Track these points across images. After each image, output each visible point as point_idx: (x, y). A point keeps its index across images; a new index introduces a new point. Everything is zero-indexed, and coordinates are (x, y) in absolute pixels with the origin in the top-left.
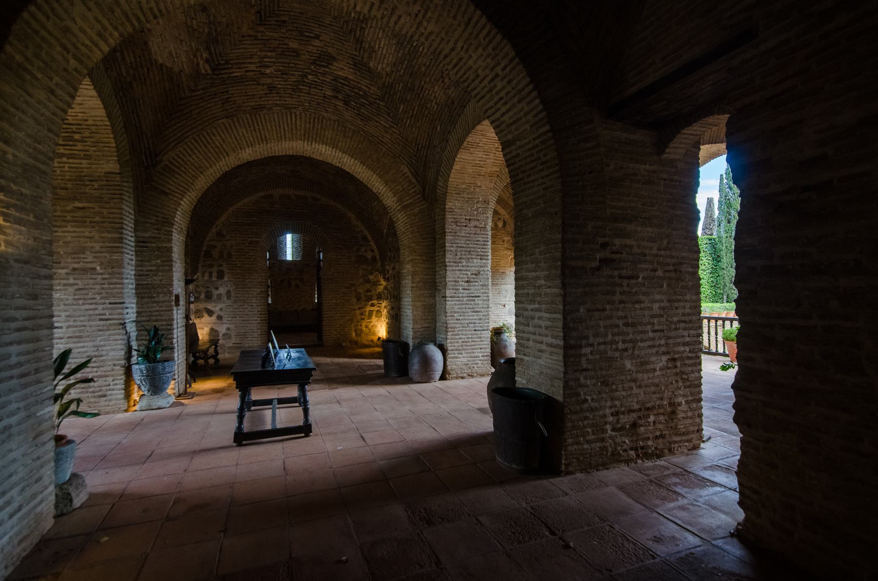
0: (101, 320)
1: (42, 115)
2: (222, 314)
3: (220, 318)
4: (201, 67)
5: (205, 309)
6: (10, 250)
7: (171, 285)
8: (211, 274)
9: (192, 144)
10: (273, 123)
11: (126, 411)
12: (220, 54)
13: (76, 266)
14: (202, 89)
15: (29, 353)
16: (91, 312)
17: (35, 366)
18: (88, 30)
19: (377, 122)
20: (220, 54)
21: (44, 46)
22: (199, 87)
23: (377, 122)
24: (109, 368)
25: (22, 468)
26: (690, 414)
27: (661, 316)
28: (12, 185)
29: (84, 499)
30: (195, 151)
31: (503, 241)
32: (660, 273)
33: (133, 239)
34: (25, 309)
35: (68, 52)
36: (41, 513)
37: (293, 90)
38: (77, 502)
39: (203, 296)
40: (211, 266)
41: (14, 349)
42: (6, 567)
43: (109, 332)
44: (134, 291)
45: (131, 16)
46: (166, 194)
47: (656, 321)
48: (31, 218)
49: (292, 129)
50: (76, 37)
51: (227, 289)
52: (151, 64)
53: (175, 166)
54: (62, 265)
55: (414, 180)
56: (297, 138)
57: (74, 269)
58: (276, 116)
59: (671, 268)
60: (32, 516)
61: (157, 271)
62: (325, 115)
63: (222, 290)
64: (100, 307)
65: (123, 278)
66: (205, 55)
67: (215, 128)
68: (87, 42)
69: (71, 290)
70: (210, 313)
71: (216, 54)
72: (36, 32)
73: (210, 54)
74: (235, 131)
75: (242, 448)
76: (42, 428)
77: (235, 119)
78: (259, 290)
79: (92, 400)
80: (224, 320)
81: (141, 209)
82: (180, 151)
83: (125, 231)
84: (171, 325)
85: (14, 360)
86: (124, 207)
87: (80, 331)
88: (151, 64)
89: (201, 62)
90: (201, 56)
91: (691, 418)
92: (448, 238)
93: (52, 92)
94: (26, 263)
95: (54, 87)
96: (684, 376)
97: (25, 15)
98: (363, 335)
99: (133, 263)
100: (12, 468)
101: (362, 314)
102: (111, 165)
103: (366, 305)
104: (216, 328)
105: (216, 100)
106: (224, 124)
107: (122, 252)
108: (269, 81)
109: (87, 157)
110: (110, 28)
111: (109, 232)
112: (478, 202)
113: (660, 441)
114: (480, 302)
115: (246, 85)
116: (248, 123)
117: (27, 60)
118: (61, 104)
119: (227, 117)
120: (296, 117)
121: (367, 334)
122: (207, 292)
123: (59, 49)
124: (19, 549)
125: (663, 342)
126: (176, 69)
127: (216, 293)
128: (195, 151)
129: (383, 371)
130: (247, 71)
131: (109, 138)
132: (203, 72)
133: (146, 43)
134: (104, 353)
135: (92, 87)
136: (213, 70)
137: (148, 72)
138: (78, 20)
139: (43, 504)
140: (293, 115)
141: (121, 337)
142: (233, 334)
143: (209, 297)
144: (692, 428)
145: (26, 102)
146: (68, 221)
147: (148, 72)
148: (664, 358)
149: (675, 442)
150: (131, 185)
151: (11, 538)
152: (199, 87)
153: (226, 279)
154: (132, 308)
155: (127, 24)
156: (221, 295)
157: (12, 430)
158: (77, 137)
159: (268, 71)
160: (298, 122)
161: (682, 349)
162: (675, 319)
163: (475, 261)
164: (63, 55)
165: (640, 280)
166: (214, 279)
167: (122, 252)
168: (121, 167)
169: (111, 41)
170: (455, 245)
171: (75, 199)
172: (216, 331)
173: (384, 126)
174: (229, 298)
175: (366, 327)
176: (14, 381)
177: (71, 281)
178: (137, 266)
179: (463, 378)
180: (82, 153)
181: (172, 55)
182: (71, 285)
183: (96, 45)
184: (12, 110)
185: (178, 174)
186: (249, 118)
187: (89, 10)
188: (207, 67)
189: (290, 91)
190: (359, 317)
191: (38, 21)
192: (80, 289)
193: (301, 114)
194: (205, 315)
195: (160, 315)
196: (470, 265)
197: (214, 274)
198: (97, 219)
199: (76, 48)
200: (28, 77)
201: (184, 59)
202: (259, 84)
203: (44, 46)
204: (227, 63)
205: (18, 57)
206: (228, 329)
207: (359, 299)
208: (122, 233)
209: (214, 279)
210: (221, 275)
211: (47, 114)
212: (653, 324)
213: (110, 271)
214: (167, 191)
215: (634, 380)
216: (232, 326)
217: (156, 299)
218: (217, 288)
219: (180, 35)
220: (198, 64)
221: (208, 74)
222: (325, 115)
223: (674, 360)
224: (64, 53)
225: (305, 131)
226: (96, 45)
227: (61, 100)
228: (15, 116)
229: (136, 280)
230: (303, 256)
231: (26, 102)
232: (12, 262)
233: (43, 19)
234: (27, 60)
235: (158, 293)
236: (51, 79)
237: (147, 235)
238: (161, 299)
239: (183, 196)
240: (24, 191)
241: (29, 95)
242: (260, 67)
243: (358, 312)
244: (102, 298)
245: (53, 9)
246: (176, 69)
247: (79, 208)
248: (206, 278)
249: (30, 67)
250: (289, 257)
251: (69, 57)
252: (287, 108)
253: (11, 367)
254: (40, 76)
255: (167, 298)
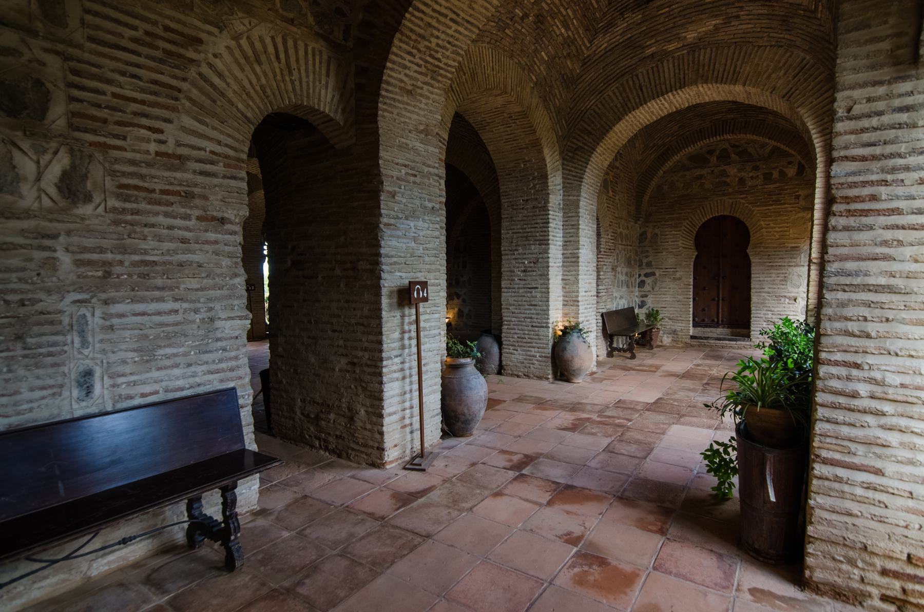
3: (464, 301)
26: (368, 426)
27: (339, 316)
31: (798, 197)
32: (338, 272)
47: (334, 320)
59: (349, 265)
91: (369, 430)
92: (505, 224)
96: (364, 384)
112: (534, 178)
113: (340, 441)
114: (539, 295)
118: (659, 90)
125: (341, 343)
144: (371, 443)
148: (344, 361)
149: (353, 449)
161: (360, 354)
162: (353, 321)
163: (533, 247)
165: (320, 279)
170: (510, 232)
179: (518, 376)
196: (527, 252)
212: (332, 324)
215: (318, 375)
223: (353, 364)
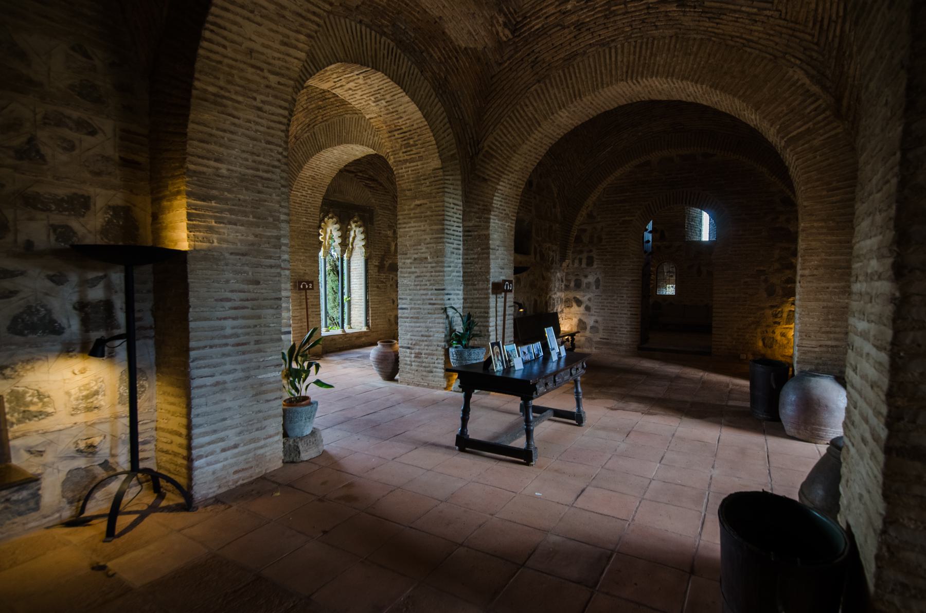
0: (430, 304)
1: (256, 131)
2: (590, 304)
3: (588, 309)
4: (501, 34)
5: (575, 298)
6: (225, 245)
7: (488, 273)
8: (580, 263)
9: (507, 122)
10: (588, 70)
11: (445, 389)
12: (515, 11)
13: (416, 256)
14: (509, 59)
15: (244, 327)
16: (424, 297)
17: (256, 338)
18: (270, 43)
19: (735, 11)
20: (515, 11)
21: (234, 72)
22: (505, 58)
23: (735, 11)
24: (434, 348)
25: (238, 416)
28: (226, 193)
29: (313, 456)
30: (510, 129)
33: (461, 229)
34: (240, 291)
35: (262, 70)
36: (263, 456)
37: (606, 17)
38: (305, 456)
39: (572, 284)
40: (581, 252)
41: (229, 323)
42: (220, 487)
43: (435, 316)
44: (461, 279)
45: (304, 13)
46: (485, 180)
48: (251, 219)
49: (611, 71)
50: (263, 54)
51: (596, 277)
52: (457, 52)
53: (493, 150)
54: (408, 256)
55: (815, 89)
56: (617, 81)
57: (415, 259)
58: (591, 60)
60: (251, 455)
61: (478, 259)
62: (656, 33)
63: (591, 279)
64: (430, 292)
65: (444, 267)
66: (501, 20)
67: (528, 98)
68: (277, 55)
69: (413, 276)
70: (579, 303)
71: (510, 13)
72: (220, 62)
73: (505, 15)
74: (547, 95)
75: (462, 454)
76: (264, 388)
77: (547, 81)
78: (630, 279)
79: (424, 373)
80: (592, 312)
81: (468, 199)
82: (498, 134)
83: (446, 222)
84: (488, 313)
85: (228, 331)
86: (446, 199)
87: (418, 313)
88: (457, 52)
89: (500, 29)
90: (498, 22)
93: (260, 109)
94: (243, 255)
95: (261, 105)
97: (201, 52)
98: (776, 347)
99: (461, 252)
100: (227, 414)
101: (775, 316)
102: (436, 163)
103: (783, 303)
104: (585, 320)
105: (525, 65)
106: (536, 90)
107: (443, 242)
108: (574, 18)
109: (421, 158)
110: (294, 34)
111: (436, 224)
115: (550, 36)
116: (561, 81)
117: (221, 88)
119: (539, 81)
120: (616, 52)
121: (784, 346)
122: (576, 280)
123: (251, 70)
124: (236, 477)
126: (480, 48)
127: (585, 281)
128: (510, 129)
129: (748, 405)
130: (547, 18)
131: (429, 136)
132: (505, 39)
133: (444, 33)
134: (431, 334)
135: (404, 94)
136: (513, 32)
137: (458, 61)
138: (254, 37)
139: (267, 449)
140: (613, 51)
141: (442, 321)
142: (601, 328)
143: (578, 286)
145: (234, 124)
146: (411, 218)
147: (458, 61)
150: (460, 177)
151: (224, 466)
152: (505, 58)
153: (595, 266)
154: (458, 294)
155: (307, 23)
156: (590, 283)
157: (226, 385)
158: (411, 142)
159: (569, 7)
160: (619, 58)
164: (258, 75)
166: (584, 265)
167: (443, 242)
168: (443, 162)
169: (301, 45)
171: (415, 198)
172: (584, 323)
173: (749, 14)
174: (597, 287)
175: (783, 335)
176: (229, 348)
177: (413, 270)
178: (464, 254)
180: (417, 156)
181: (471, 34)
182: (413, 273)
183: (289, 55)
184: (221, 133)
185: (497, 158)
186: (562, 74)
187: (260, 25)
188: (507, 32)
189: (601, 21)
190: (771, 320)
191: (216, 53)
192: (418, 277)
193: (623, 45)
194: (574, 304)
195: (479, 303)
197: (584, 261)
198: (429, 213)
199: (269, 64)
200: (229, 103)
201: (483, 33)
202: (564, 28)
203: (234, 72)
204: (525, 18)
205: (211, 89)
206: (596, 322)
207: (771, 292)
208: (443, 225)
209: (584, 265)
210: (590, 262)
211: (262, 129)
213: (436, 259)
214: (487, 177)
216: (599, 319)
217: (477, 287)
218: (586, 276)
219: (469, 10)
220: (498, 33)
221: (509, 40)
222: (656, 33)
224: (258, 72)
225: (628, 67)
226: (289, 55)
227: (273, 114)
228: (223, 138)
229: (463, 268)
230: (718, 236)
231: (234, 124)
232: (227, 255)
233: (220, 49)
234: (221, 88)
235: (479, 281)
236: (255, 99)
237: (471, 224)
238: (481, 287)
239: (499, 180)
240: (242, 197)
241: (234, 117)
242: (560, 5)
243: (769, 312)
244: (431, 285)
245: (225, 38)
246: (480, 48)
247: (418, 205)
248: (576, 265)
249: (227, 94)
250: (705, 237)
251: (266, 74)
252: (604, 45)
253: (225, 337)
254: (240, 99)
255: (485, 286)
